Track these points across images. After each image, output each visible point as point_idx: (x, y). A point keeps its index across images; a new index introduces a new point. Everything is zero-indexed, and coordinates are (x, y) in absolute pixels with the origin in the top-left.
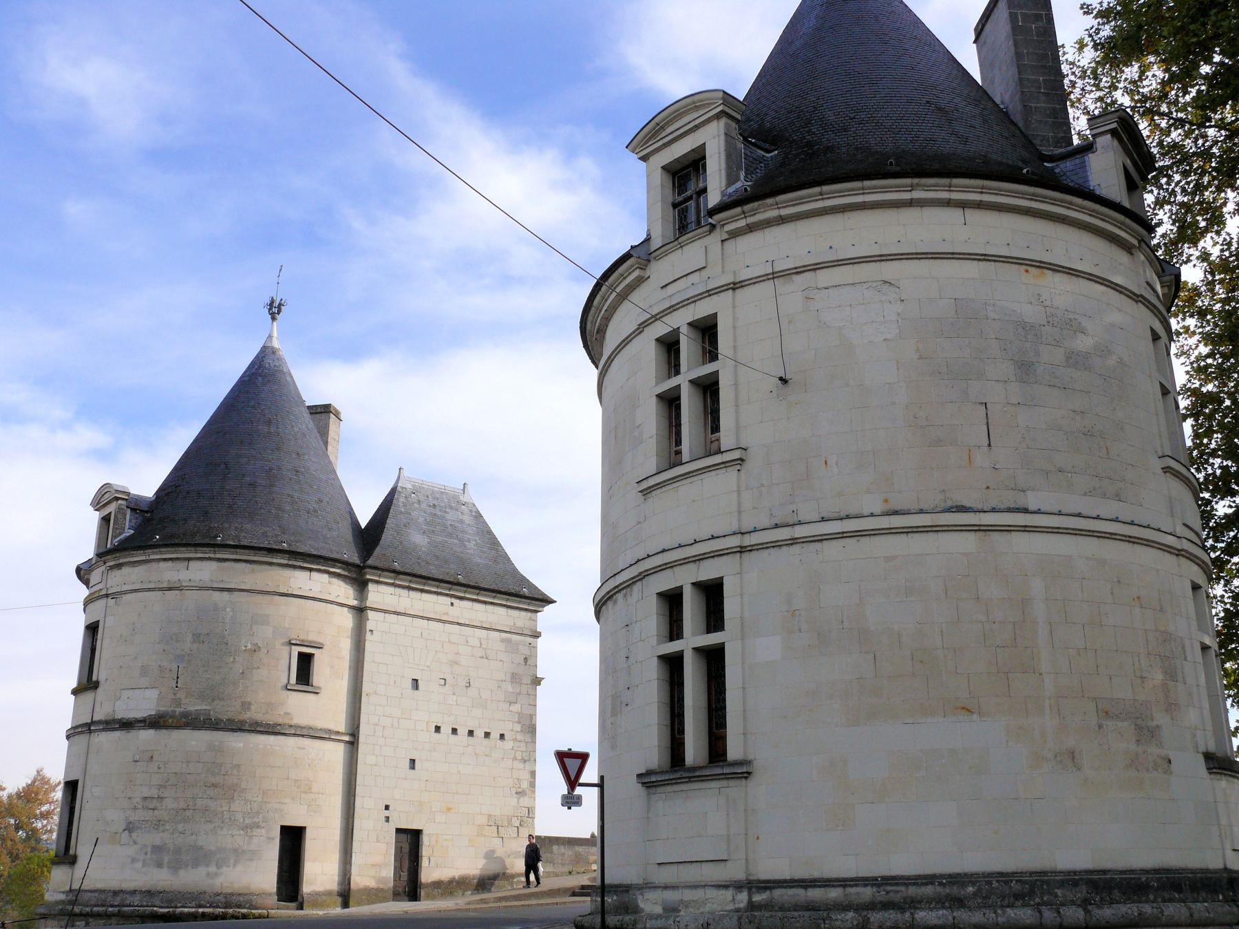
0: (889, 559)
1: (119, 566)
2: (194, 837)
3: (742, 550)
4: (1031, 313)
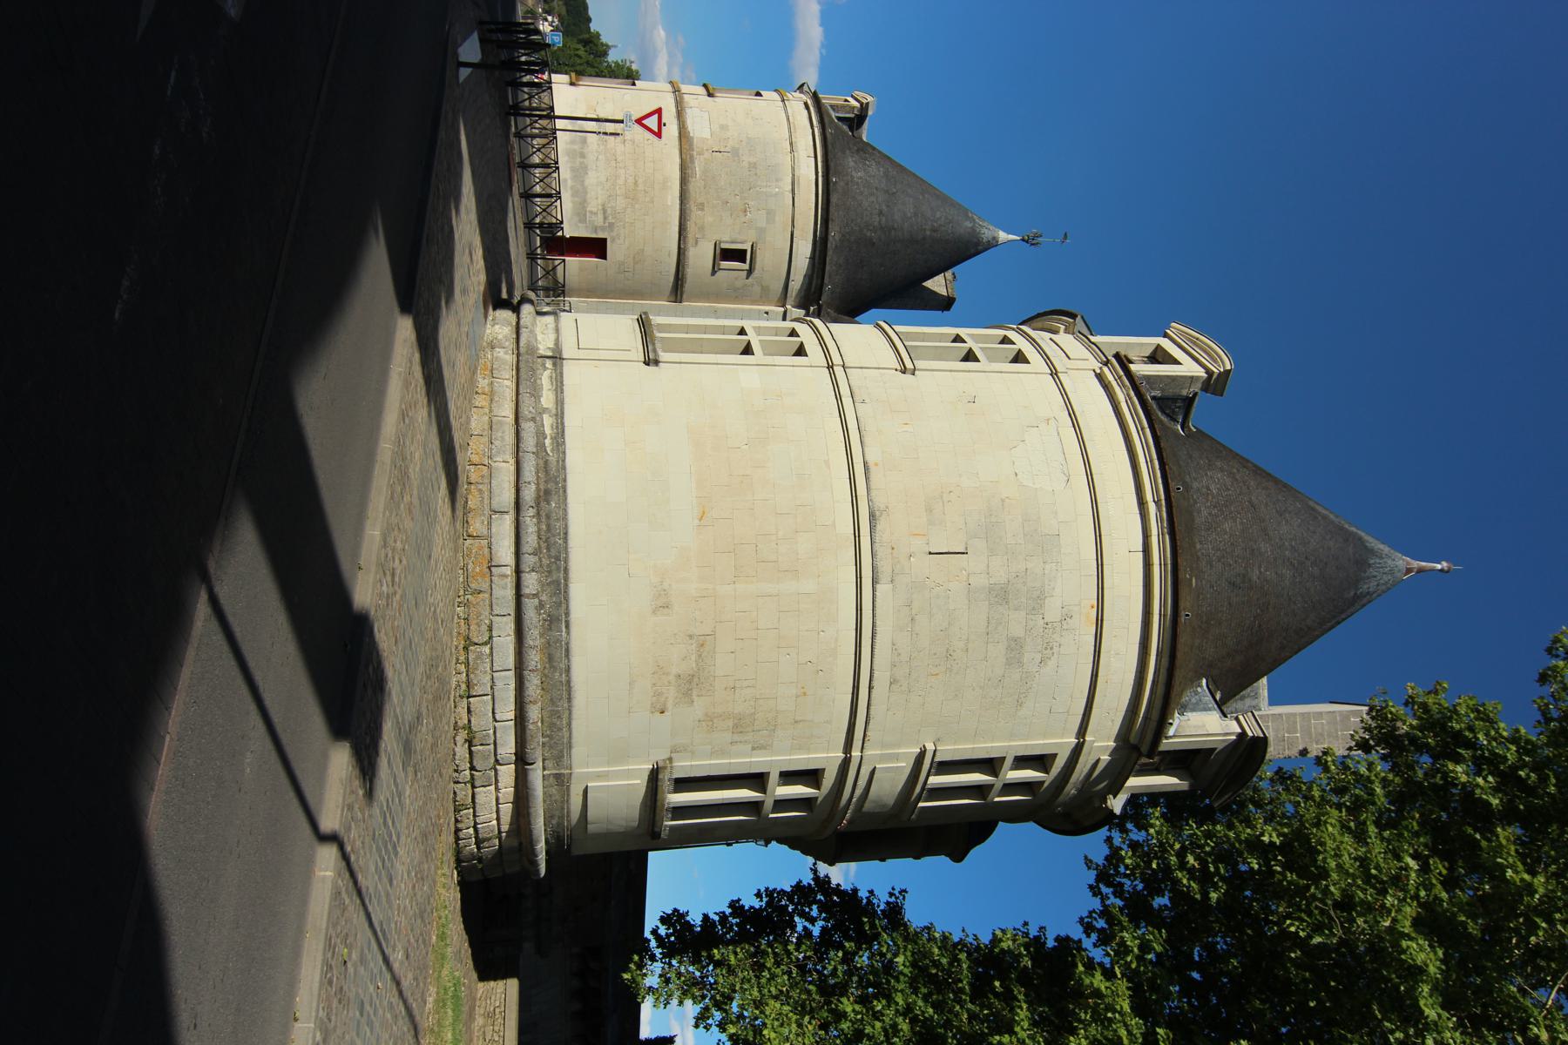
0: (827, 463)
1: (807, 107)
3: (830, 367)
4: (1052, 612)
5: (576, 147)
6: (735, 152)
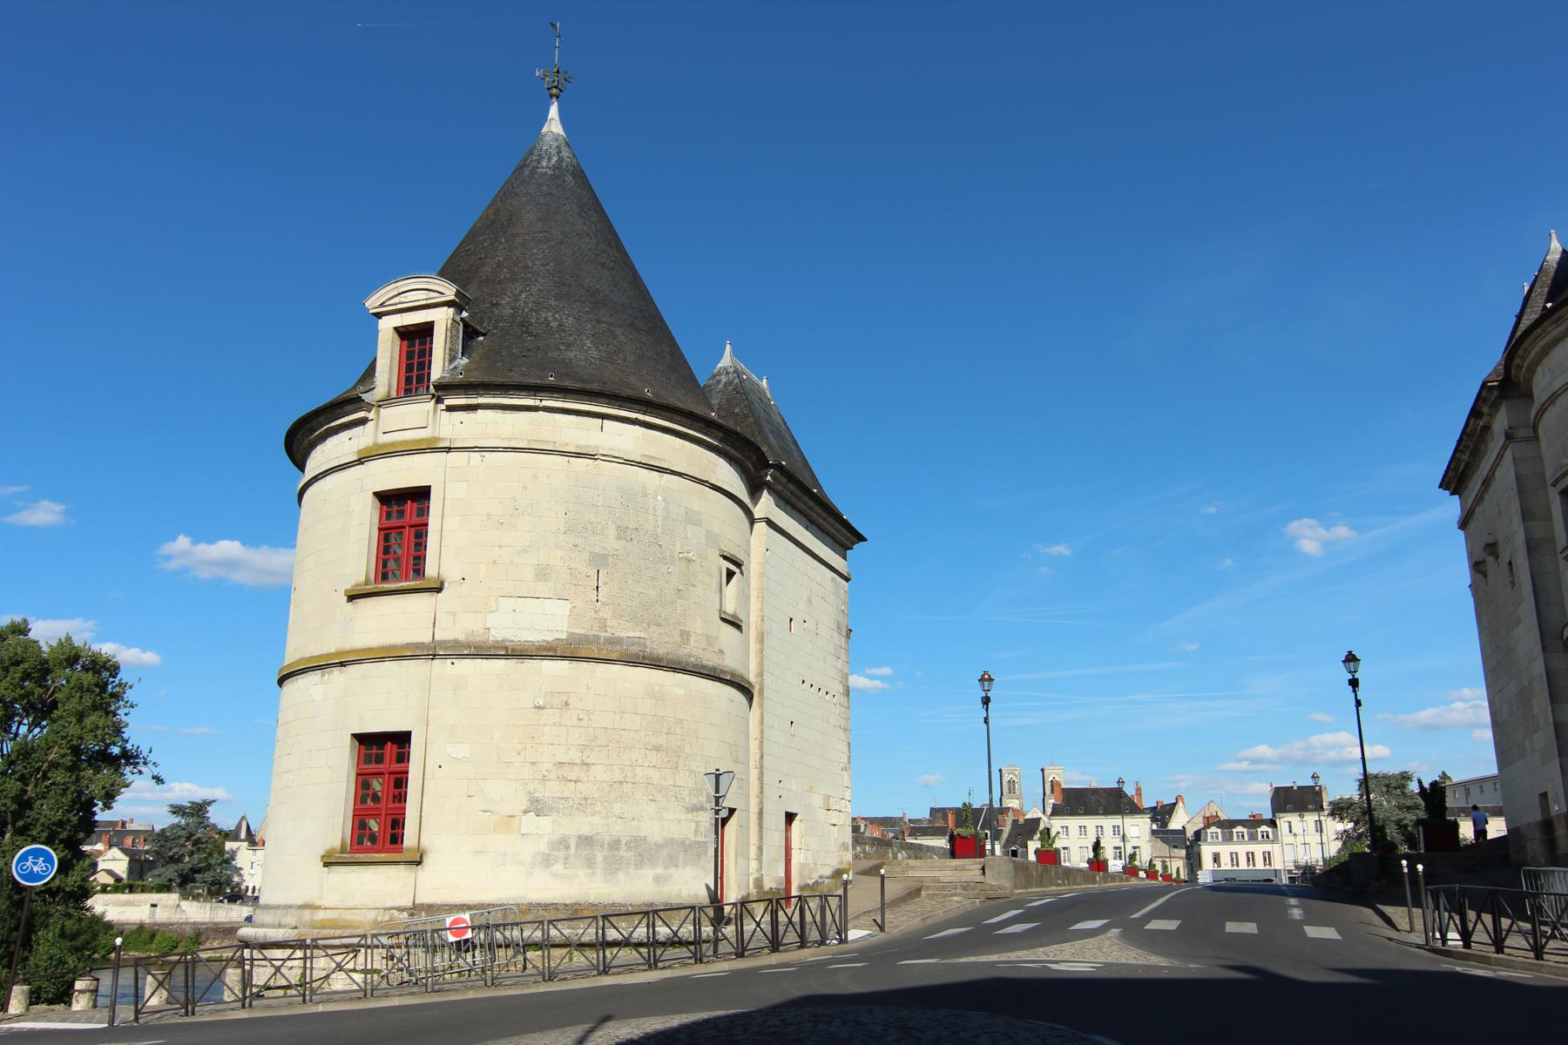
2: (635, 823)
5: (599, 856)
6: (599, 561)
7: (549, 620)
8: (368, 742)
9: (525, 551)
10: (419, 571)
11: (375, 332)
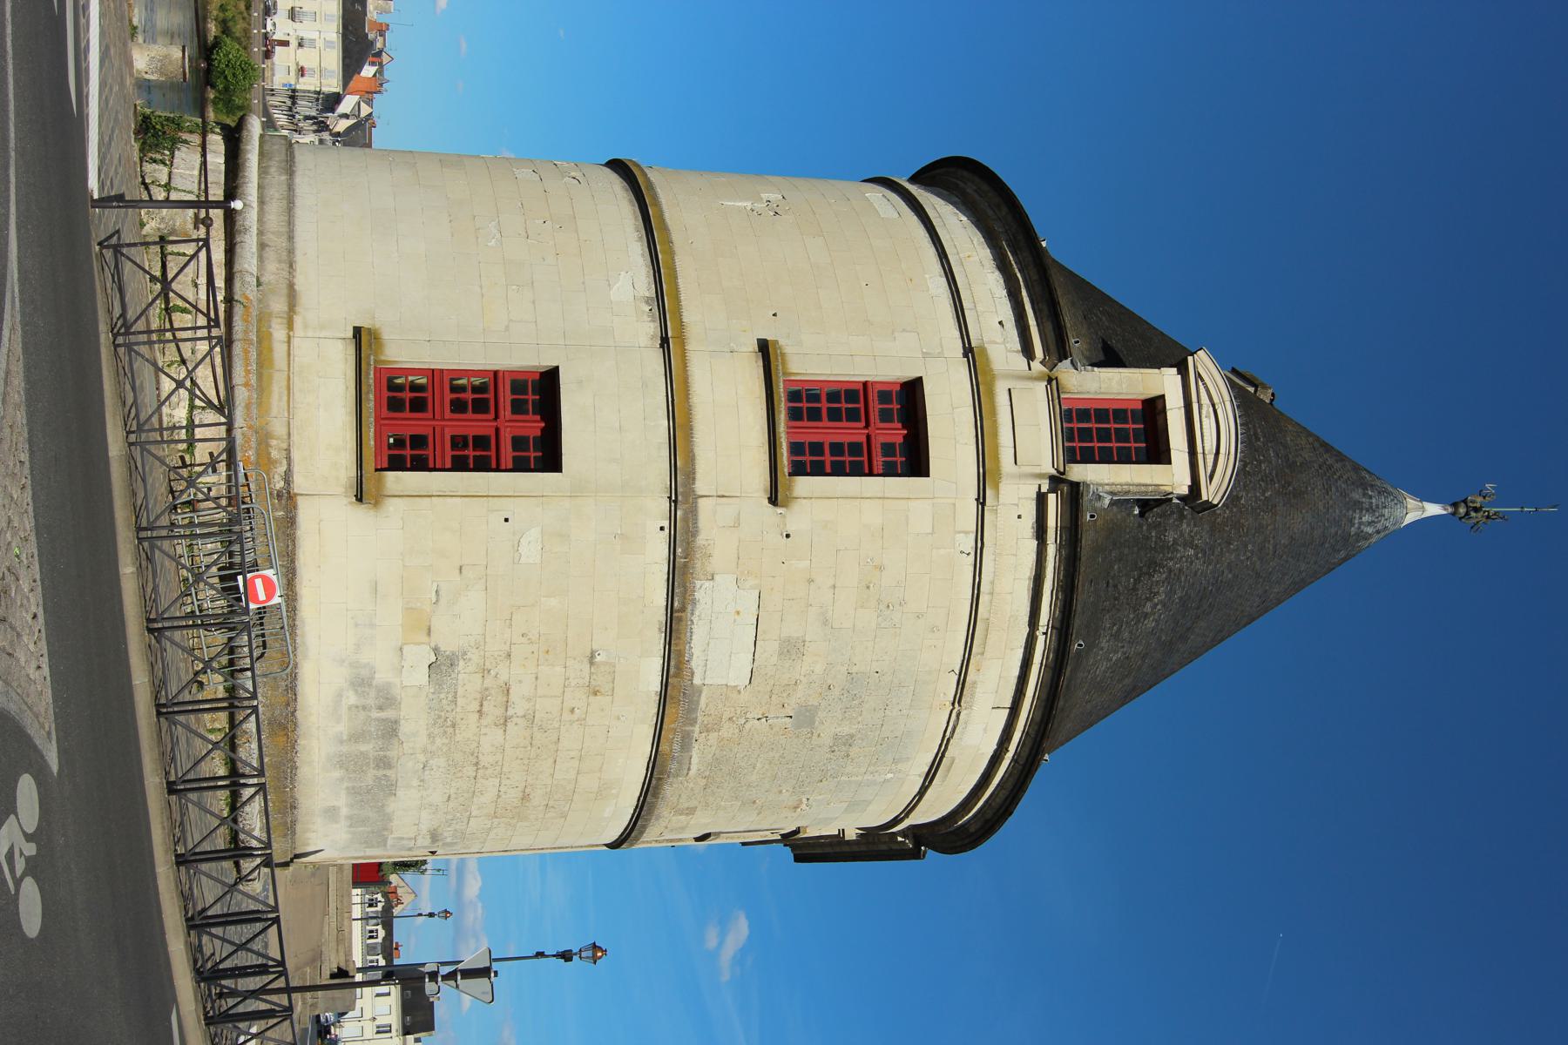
2: (415, 783)
6: (805, 718)
7: (719, 657)
8: (543, 391)
9: (825, 622)
10: (798, 470)
11: (1157, 364)
